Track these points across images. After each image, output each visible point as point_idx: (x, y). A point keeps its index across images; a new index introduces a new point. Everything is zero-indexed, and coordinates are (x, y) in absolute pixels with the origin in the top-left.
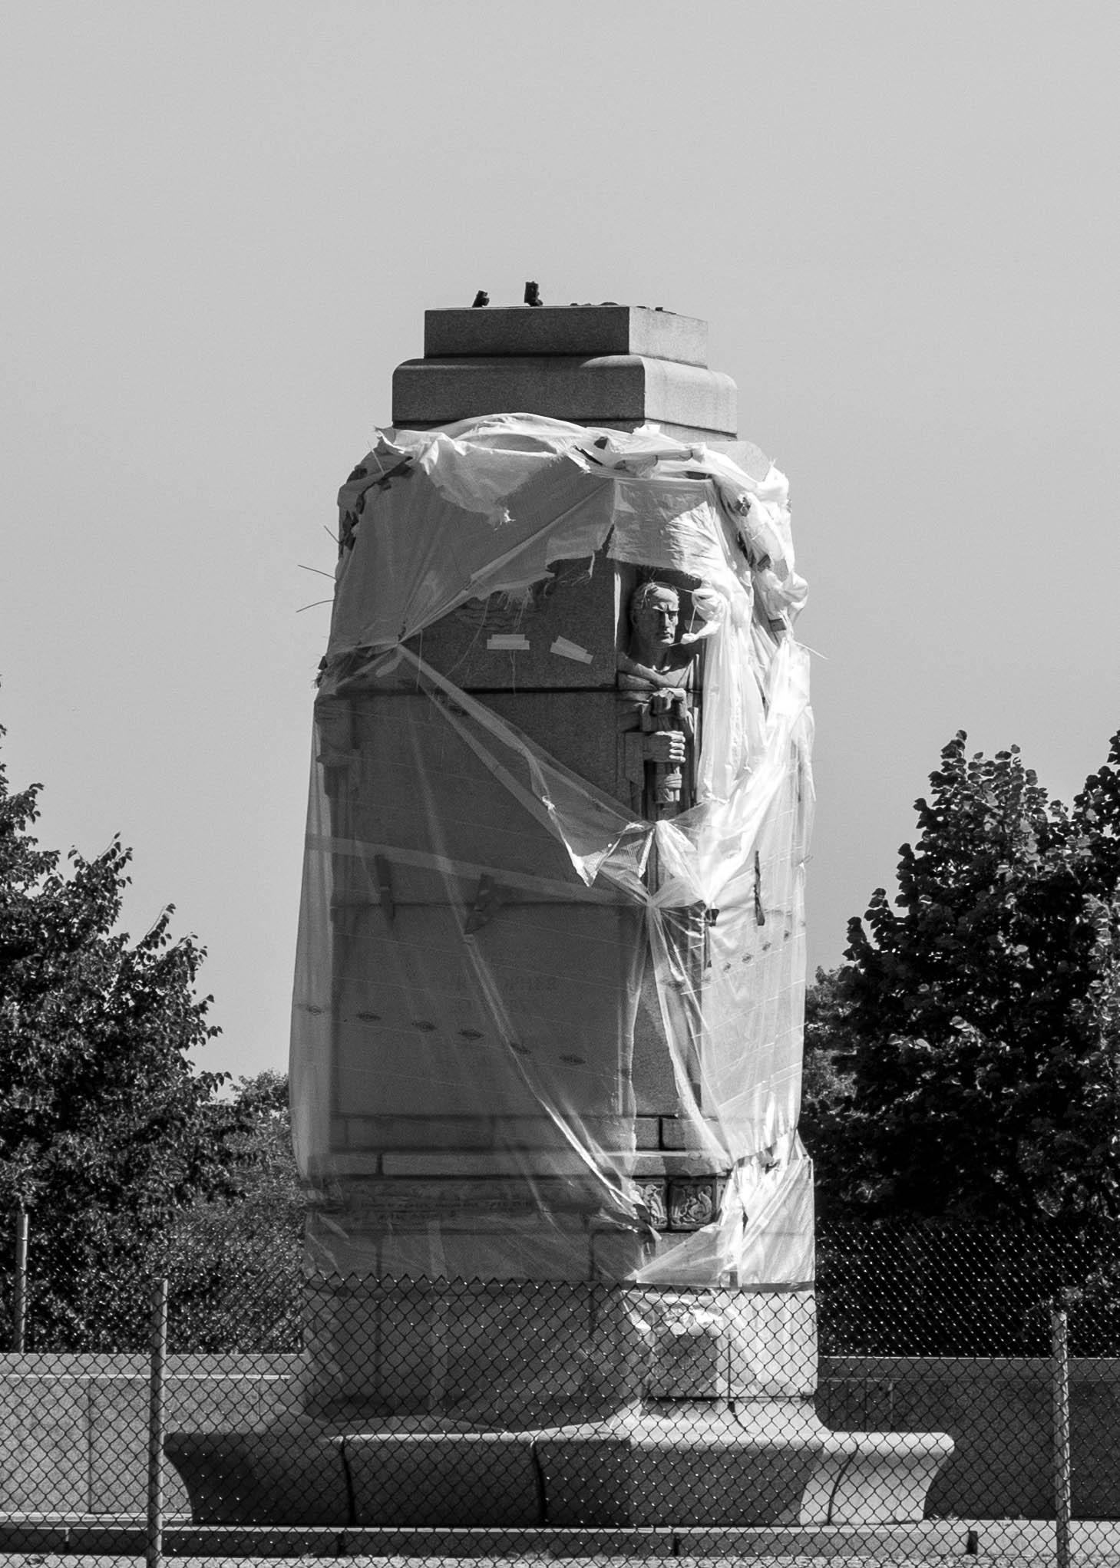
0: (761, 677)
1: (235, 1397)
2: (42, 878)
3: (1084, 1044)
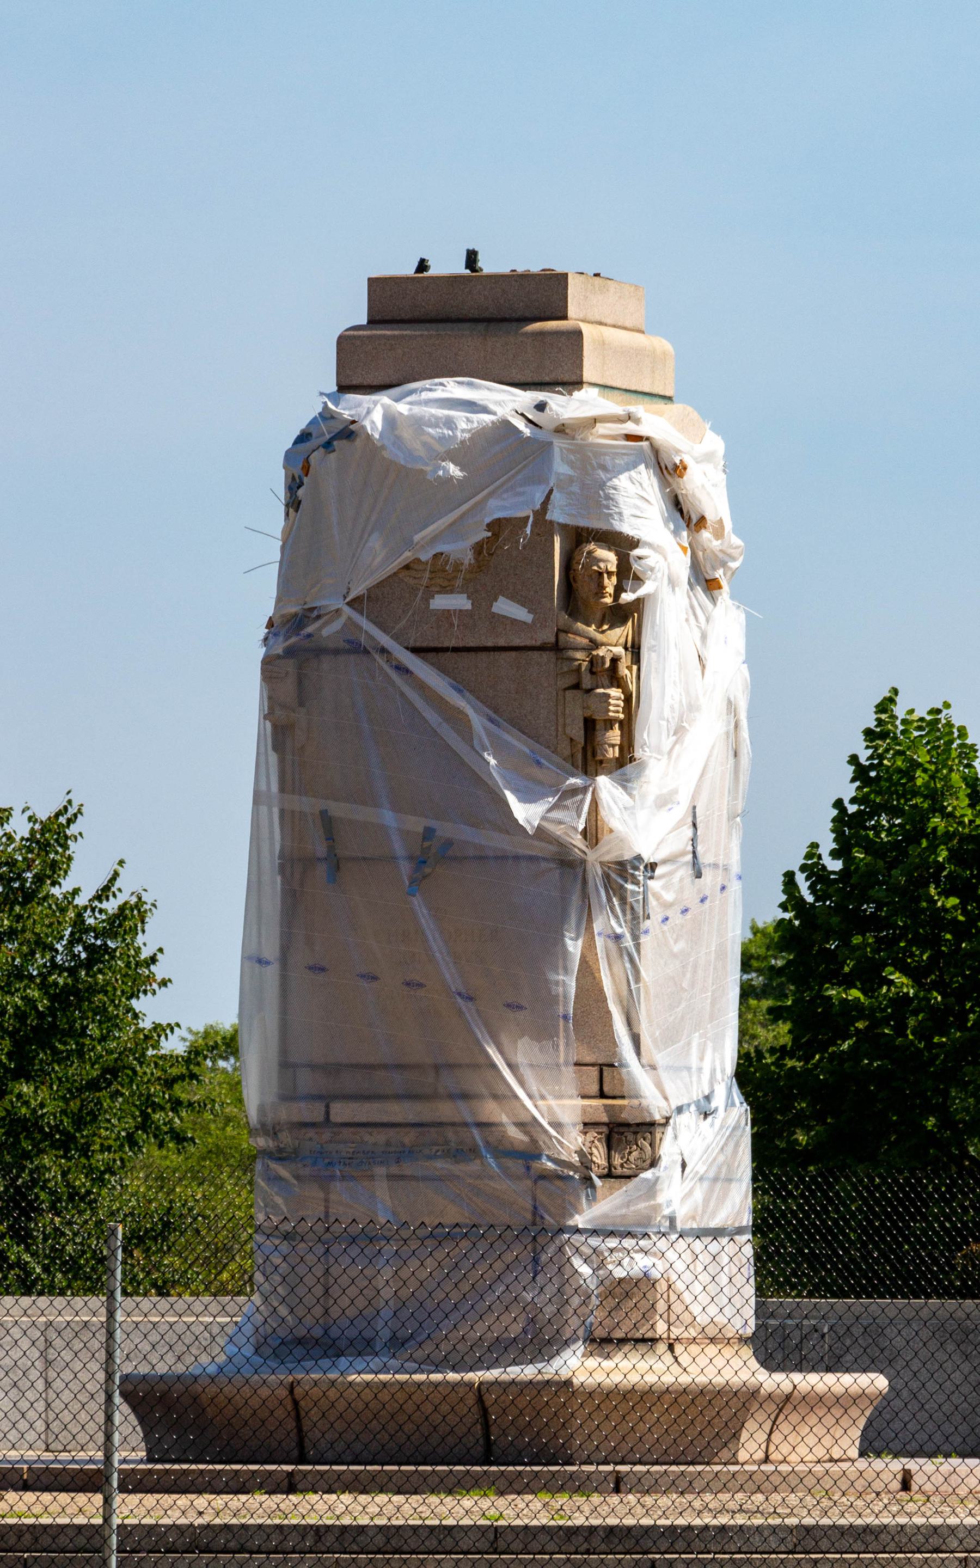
1: (188, 1339)
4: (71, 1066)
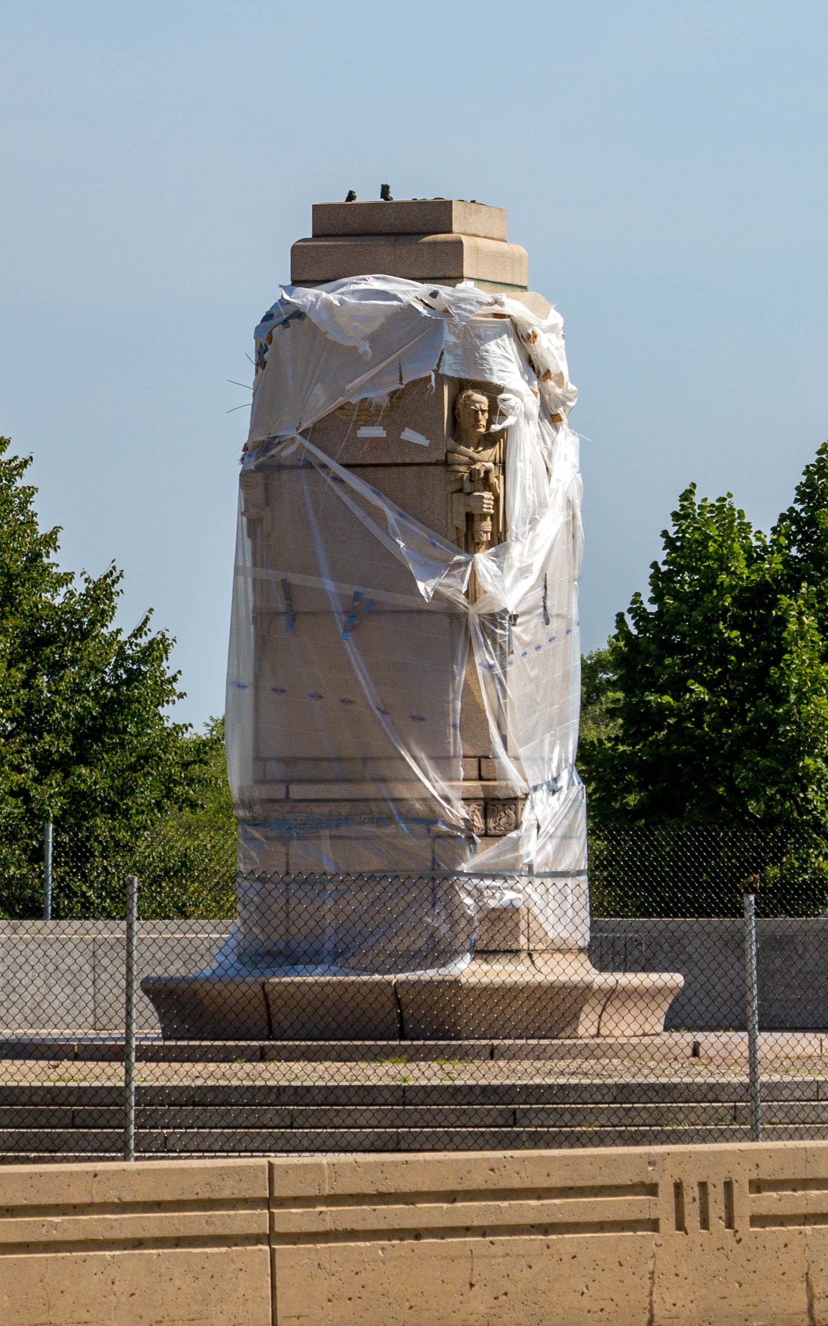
0: (546, 454)
1: (191, 950)
2: (63, 591)
3: (779, 699)
4: (116, 754)
